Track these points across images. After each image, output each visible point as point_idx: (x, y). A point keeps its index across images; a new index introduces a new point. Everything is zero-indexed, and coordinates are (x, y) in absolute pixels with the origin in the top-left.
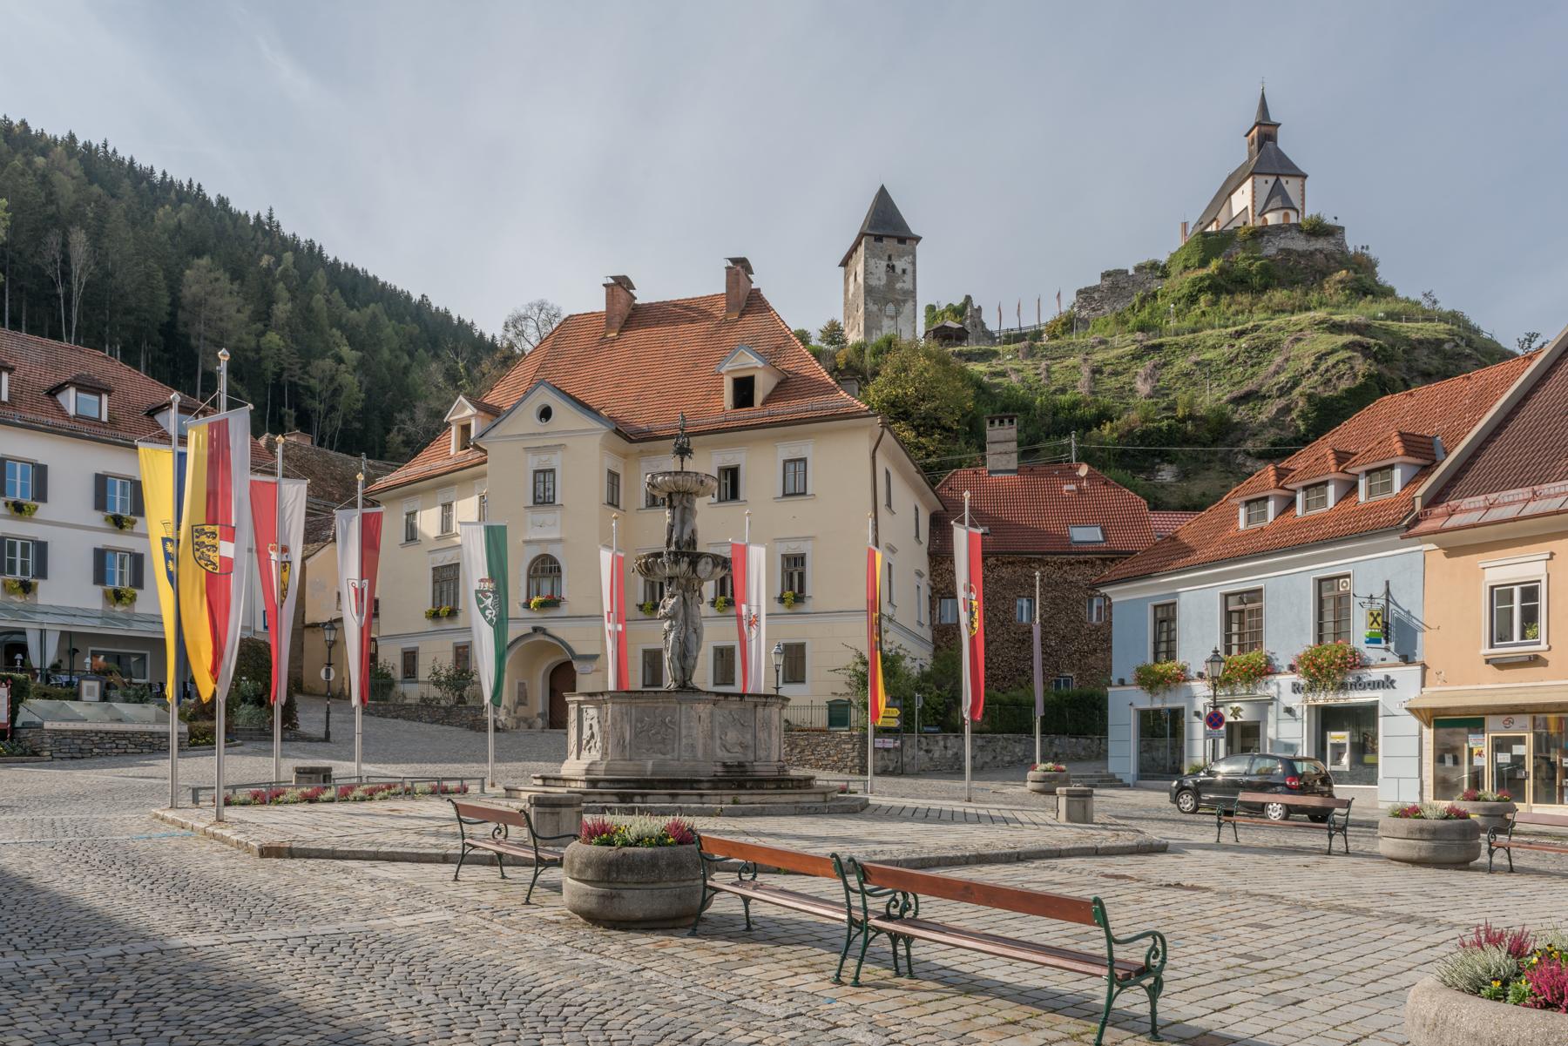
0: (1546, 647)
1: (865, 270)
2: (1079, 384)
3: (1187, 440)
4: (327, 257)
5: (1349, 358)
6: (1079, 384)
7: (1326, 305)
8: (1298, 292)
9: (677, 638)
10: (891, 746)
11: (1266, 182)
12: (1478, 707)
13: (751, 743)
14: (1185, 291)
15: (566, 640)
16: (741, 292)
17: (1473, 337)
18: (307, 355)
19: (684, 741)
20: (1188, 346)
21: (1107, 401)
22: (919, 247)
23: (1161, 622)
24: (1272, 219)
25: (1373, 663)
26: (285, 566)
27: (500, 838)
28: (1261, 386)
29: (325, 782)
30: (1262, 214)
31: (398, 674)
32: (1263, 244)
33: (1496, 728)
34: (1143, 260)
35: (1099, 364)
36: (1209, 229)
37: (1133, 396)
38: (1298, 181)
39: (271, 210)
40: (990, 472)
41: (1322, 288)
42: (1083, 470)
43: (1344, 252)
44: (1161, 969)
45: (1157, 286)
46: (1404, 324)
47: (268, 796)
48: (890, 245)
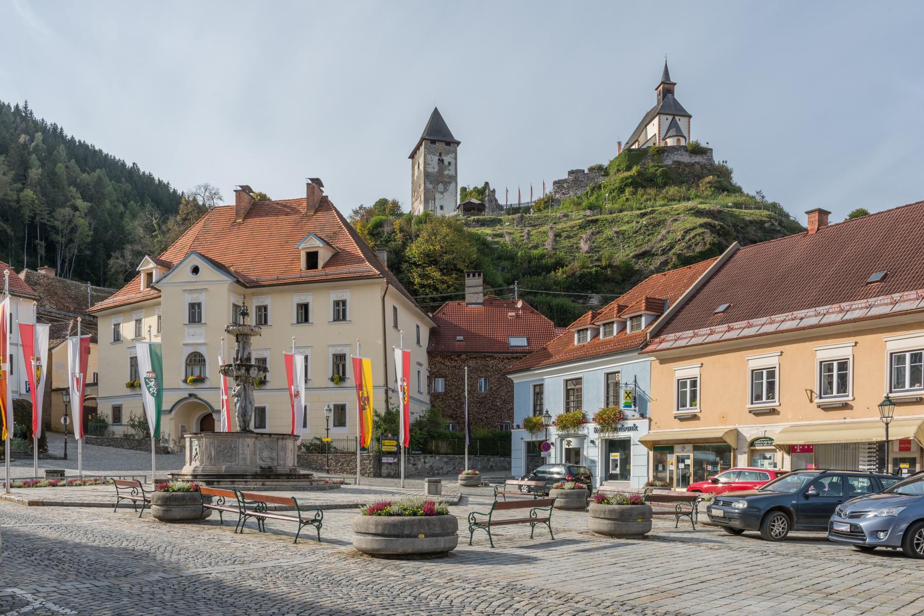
0: (778, 404)
1: (425, 162)
2: (546, 243)
3: (607, 280)
4: (66, 136)
5: (703, 233)
6: (546, 243)
7: (699, 197)
8: (684, 189)
9: (241, 406)
10: (392, 461)
11: (667, 119)
12: (663, 441)
13: (276, 457)
14: (617, 185)
15: (208, 401)
16: (316, 199)
17: (783, 219)
18: (53, 205)
19: (241, 456)
20: (613, 222)
21: (562, 254)
22: (459, 149)
23: (538, 394)
24: (671, 142)
25: (629, 418)
26: (39, 367)
27: (135, 494)
28: (652, 248)
29: (61, 476)
30: (664, 139)
31: (110, 420)
32: (664, 158)
33: (678, 452)
34: (594, 164)
35: (560, 231)
36: (633, 147)
37: (579, 252)
38: (686, 119)
39: (26, 102)
40: (467, 304)
41: (698, 186)
42: (520, 304)
43: (712, 164)
44: (321, 520)
45: (603, 181)
46: (744, 210)
47: (32, 483)
48: (440, 146)
